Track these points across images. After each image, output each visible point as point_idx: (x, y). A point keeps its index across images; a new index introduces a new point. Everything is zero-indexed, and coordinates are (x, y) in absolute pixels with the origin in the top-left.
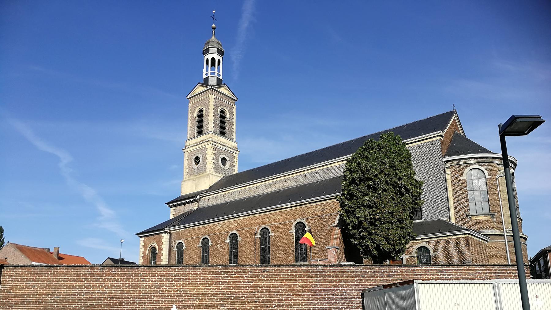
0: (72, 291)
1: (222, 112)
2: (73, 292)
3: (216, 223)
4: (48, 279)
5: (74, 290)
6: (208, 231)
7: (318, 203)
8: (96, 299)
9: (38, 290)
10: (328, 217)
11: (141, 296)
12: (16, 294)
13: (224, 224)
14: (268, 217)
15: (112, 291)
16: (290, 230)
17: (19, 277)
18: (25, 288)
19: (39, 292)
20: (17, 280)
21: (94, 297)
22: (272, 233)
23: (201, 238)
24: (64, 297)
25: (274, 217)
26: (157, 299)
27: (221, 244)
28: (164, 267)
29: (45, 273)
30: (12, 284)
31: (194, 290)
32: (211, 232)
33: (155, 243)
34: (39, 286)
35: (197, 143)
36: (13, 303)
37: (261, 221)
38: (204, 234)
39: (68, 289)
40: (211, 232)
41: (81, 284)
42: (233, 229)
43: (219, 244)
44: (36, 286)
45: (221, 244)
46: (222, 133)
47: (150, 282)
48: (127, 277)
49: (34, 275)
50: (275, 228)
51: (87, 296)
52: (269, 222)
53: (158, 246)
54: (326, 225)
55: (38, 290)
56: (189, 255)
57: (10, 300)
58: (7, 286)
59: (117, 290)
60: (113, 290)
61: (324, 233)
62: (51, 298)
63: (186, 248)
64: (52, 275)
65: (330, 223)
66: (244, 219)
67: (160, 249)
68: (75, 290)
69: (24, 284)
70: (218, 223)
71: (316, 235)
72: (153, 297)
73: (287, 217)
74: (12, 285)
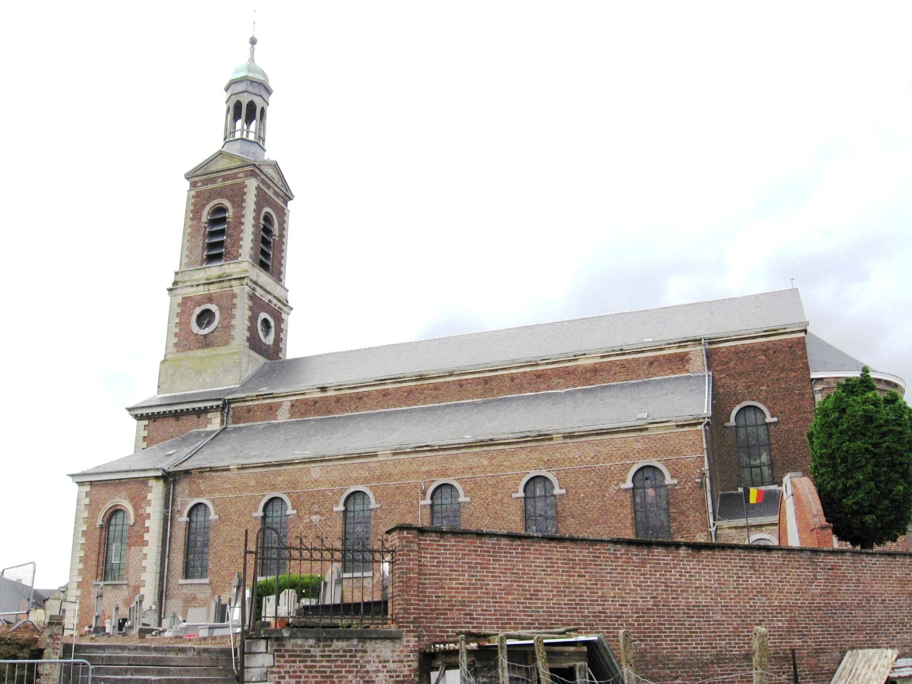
0: (565, 596)
1: (267, 218)
2: (566, 598)
3: (307, 466)
4: (514, 566)
5: (568, 596)
6: (283, 481)
7: (584, 439)
8: (612, 617)
9: (496, 594)
10: (610, 469)
11: (691, 612)
12: (452, 601)
13: (331, 468)
14: (455, 460)
15: (638, 599)
16: (513, 492)
17: (453, 558)
18: (467, 586)
19: (498, 596)
20: (449, 567)
21: (608, 611)
22: (466, 496)
23: (263, 498)
24: (550, 612)
25: (473, 461)
26: (719, 618)
27: (321, 514)
28: (785, 552)
29: (505, 553)
30: (438, 574)
31: (776, 599)
32: (294, 484)
33: (126, 502)
34: (498, 583)
35: (211, 279)
36: (448, 623)
37: (434, 467)
38: (273, 487)
39: (555, 593)
40: (294, 484)
41: (578, 580)
42: (356, 481)
43: (316, 513)
44: (491, 583)
45: (322, 515)
46: (264, 266)
47: (703, 581)
48: (661, 567)
49: (484, 555)
50: (474, 486)
51: (594, 608)
52: (458, 471)
53: (136, 509)
54: (606, 487)
55: (496, 594)
56: (227, 535)
57: (442, 614)
58: (430, 579)
59: (647, 598)
60: (640, 598)
61: (599, 501)
62: (524, 611)
63: (217, 517)
64: (519, 558)
65: (615, 482)
66: (389, 463)
67: (141, 515)
68: (570, 596)
69: (465, 576)
70: (313, 465)
71: (581, 506)
72: (711, 615)
73: (505, 463)
74: (441, 579)
